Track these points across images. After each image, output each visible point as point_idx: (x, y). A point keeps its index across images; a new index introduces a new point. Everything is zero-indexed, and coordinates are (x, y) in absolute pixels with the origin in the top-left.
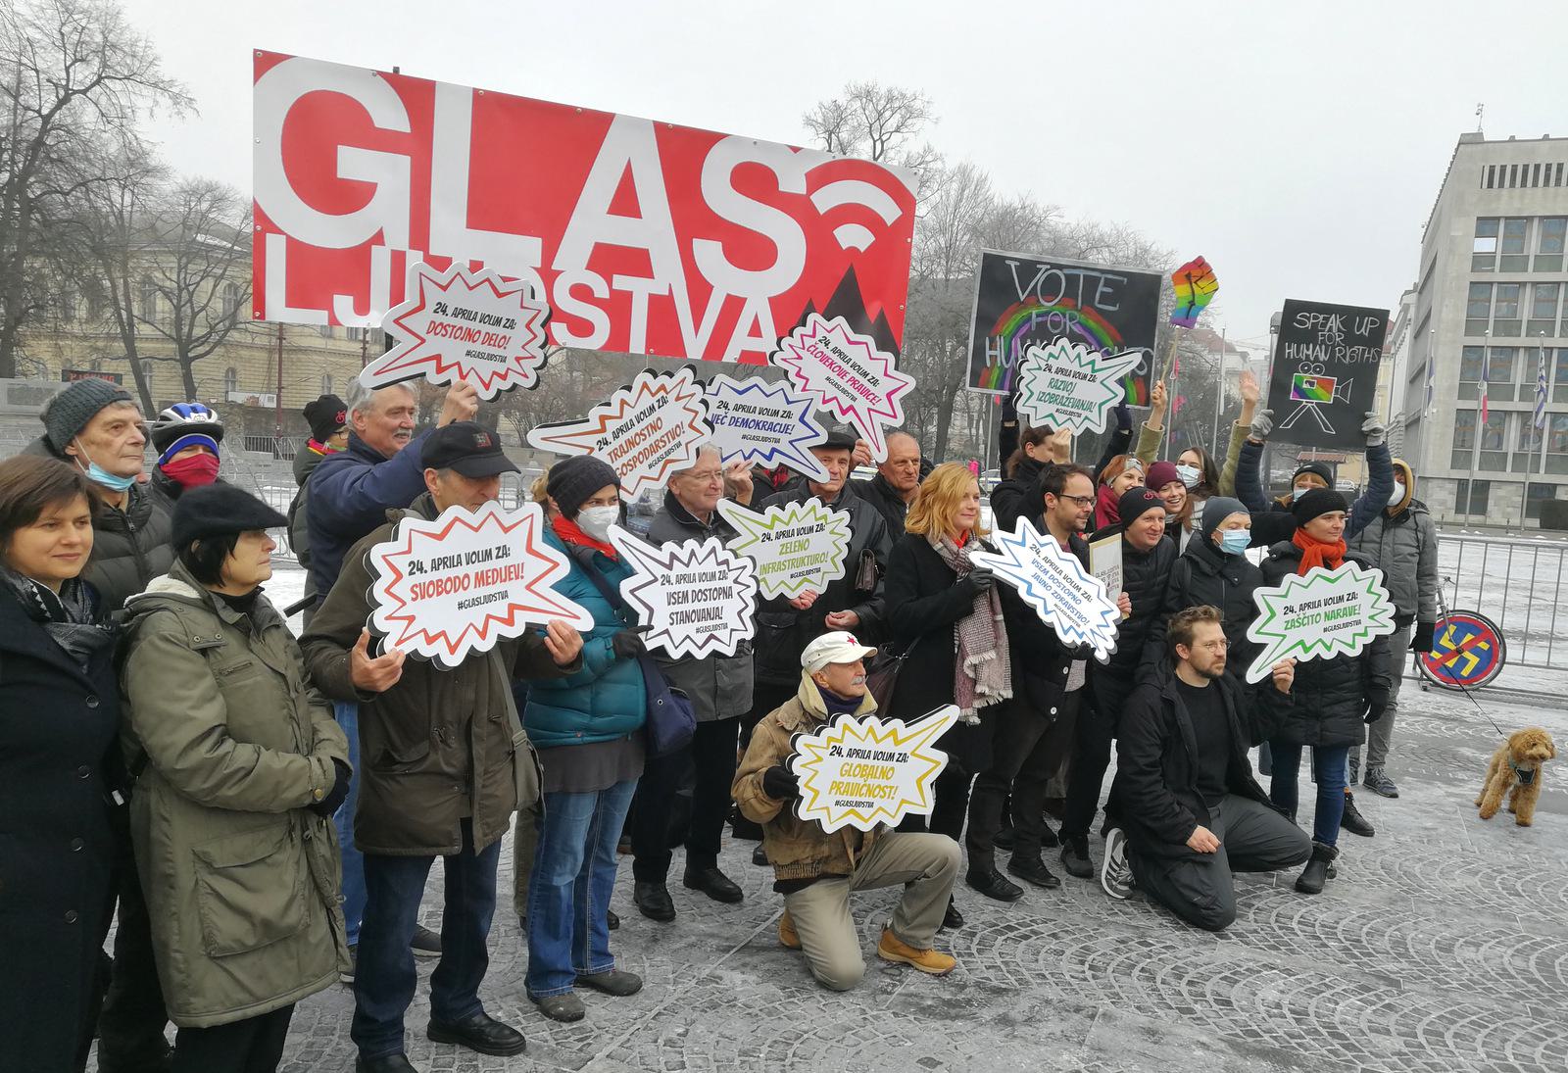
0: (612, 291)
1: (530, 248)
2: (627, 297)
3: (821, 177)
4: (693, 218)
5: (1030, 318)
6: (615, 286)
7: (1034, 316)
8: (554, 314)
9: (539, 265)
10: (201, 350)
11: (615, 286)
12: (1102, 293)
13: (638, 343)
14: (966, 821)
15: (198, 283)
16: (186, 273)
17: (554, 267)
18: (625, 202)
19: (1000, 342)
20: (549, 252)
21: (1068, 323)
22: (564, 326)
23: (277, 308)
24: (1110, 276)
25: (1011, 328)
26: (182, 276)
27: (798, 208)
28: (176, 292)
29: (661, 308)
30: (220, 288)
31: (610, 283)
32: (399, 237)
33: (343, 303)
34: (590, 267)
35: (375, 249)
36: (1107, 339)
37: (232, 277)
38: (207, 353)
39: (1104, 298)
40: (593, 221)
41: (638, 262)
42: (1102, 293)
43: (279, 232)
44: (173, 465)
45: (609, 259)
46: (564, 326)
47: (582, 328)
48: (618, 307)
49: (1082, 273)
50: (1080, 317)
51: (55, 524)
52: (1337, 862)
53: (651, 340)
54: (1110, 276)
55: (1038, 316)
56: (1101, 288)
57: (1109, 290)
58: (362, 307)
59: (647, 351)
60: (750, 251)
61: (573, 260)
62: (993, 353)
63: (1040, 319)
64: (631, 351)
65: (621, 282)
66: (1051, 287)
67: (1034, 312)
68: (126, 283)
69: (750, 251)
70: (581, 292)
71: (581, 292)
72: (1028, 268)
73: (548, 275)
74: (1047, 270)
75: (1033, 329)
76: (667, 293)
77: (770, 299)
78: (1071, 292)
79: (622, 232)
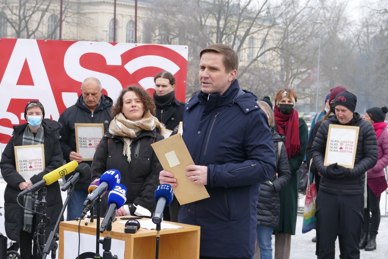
14: (32, 252)
15: (30, 16)
16: (25, 9)
18: (25, 78)
26: (22, 12)
28: (18, 22)
30: (45, 19)
34: (9, 110)
37: (53, 10)
52: (329, 93)
79: (25, 93)
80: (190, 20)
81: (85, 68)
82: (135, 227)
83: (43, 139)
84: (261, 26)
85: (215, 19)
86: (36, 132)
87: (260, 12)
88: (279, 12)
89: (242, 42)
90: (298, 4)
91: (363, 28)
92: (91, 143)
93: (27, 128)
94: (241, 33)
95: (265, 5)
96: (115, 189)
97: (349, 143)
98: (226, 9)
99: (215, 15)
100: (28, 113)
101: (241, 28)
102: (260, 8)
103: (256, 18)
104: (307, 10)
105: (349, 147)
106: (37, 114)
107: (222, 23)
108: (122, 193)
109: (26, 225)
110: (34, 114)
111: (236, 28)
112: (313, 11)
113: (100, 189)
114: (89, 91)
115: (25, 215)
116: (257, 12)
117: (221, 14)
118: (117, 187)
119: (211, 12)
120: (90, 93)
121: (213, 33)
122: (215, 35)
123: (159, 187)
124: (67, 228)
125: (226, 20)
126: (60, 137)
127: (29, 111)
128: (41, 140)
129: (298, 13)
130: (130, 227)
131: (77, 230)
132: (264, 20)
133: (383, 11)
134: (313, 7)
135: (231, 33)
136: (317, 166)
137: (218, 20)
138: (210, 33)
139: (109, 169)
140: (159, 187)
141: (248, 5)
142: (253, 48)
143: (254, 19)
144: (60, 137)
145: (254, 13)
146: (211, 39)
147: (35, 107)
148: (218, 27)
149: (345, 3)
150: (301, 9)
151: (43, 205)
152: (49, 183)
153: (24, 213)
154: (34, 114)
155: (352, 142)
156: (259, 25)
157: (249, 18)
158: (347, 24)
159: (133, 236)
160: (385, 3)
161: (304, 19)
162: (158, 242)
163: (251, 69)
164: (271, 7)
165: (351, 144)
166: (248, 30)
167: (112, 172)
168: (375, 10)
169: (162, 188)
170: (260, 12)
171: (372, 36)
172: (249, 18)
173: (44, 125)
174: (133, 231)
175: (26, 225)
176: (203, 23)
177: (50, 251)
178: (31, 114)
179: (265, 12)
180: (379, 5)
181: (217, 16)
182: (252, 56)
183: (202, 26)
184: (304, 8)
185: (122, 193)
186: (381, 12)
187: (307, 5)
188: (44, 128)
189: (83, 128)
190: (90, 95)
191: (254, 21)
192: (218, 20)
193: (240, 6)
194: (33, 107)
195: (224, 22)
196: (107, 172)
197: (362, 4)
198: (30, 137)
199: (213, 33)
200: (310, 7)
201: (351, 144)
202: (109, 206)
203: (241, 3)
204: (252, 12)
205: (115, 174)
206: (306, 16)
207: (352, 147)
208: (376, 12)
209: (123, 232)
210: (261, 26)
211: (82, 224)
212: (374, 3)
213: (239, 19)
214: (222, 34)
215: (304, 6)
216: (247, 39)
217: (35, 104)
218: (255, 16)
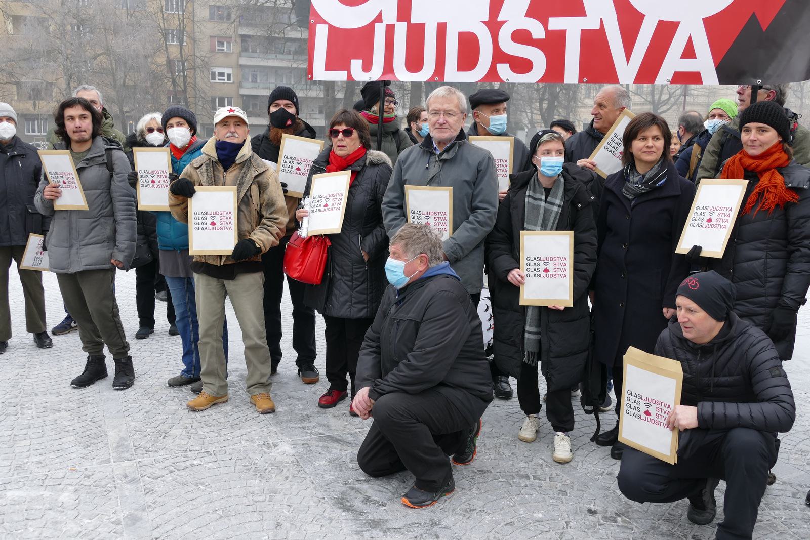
0: (547, 32)
6: (550, 28)
8: (499, 56)
9: (487, 19)
10: (665, 108)
11: (550, 28)
13: (572, 73)
17: (499, 19)
22: (507, 66)
23: (320, 73)
29: (594, 42)
31: (545, 24)
32: (390, 16)
33: (356, 65)
35: (377, 25)
38: (668, 110)
43: (325, 22)
44: (394, 166)
46: (507, 66)
47: (522, 65)
48: (554, 45)
51: (645, 139)
58: (367, 67)
59: (581, 81)
64: (566, 81)
65: (556, 23)
70: (521, 37)
71: (521, 37)
73: (494, 25)
81: (364, 3)
83: (561, 200)
86: (550, 187)
93: (532, 180)
97: (502, 163)
105: (225, 220)
109: (528, 352)
110: (554, 153)
115: (526, 335)
126: (593, 198)
128: (558, 202)
136: (755, 376)
144: (593, 198)
147: (556, 140)
153: (524, 331)
154: (554, 153)
155: (506, 161)
165: (505, 164)
173: (566, 174)
175: (528, 352)
188: (565, 180)
194: (553, 140)
198: (538, 196)
201: (505, 164)
207: (565, 273)
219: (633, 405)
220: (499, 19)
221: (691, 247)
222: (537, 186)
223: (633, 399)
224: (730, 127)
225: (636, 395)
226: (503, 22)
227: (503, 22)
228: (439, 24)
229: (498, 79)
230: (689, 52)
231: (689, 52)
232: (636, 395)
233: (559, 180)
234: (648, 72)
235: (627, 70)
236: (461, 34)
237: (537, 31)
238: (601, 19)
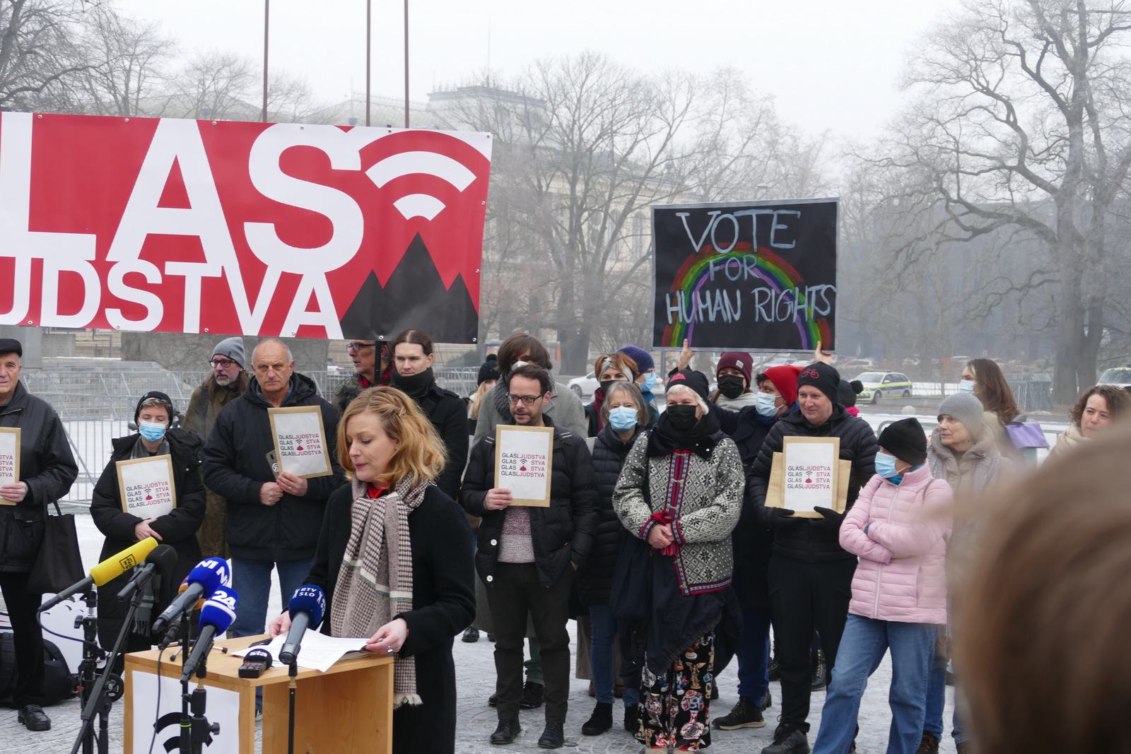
0: (164, 277)
1: (85, 244)
2: (181, 281)
3: (373, 154)
4: (242, 205)
5: (707, 269)
6: (167, 272)
7: (711, 266)
8: (108, 300)
11: (167, 272)
12: (777, 231)
17: (109, 259)
19: (681, 297)
20: (103, 247)
21: (746, 268)
24: (783, 212)
25: (690, 281)
27: (352, 183)
29: (215, 290)
31: (162, 269)
36: (787, 281)
39: (780, 236)
40: (143, 215)
41: (190, 248)
42: (777, 231)
45: (159, 248)
47: (135, 311)
48: (172, 291)
49: (754, 213)
50: (757, 260)
53: (204, 320)
54: (783, 212)
55: (715, 265)
56: (775, 226)
57: (783, 227)
60: (306, 229)
61: (126, 250)
62: (674, 309)
63: (718, 268)
65: (173, 268)
66: (724, 231)
67: (711, 261)
68: (696, 585)
69: (306, 229)
70: (134, 280)
71: (134, 280)
72: (699, 216)
73: (102, 266)
74: (718, 216)
75: (712, 279)
76: (219, 275)
77: (30, 230)
78: (745, 237)
79: (173, 223)
80: (517, 184)
82: (263, 665)
84: (657, 191)
85: (566, 180)
87: (652, 166)
88: (690, 166)
89: (620, 223)
90: (725, 150)
91: (852, 193)
92: (302, 445)
93: (136, 445)
94: (617, 207)
95: (663, 153)
96: (214, 598)
98: (586, 161)
99: (566, 174)
100: (141, 415)
101: (616, 198)
102: (653, 158)
103: (646, 177)
104: (742, 160)
106: (159, 419)
107: (580, 187)
108: (226, 605)
110: (153, 419)
111: (607, 198)
112: (754, 163)
113: (185, 597)
114: (267, 360)
116: (647, 167)
117: (578, 171)
118: (217, 592)
119: (558, 169)
120: (270, 363)
121: (563, 208)
122: (567, 213)
123: (297, 591)
124: (137, 665)
125: (587, 185)
127: (143, 412)
129: (726, 168)
130: (252, 666)
131: (156, 670)
132: (661, 182)
133: (885, 161)
134: (755, 154)
135: (597, 207)
137: (573, 183)
138: (556, 209)
139: (206, 558)
140: (297, 591)
141: (628, 153)
142: (641, 235)
143: (642, 180)
145: (641, 168)
146: (560, 218)
148: (573, 197)
149: (818, 145)
150: (732, 159)
151: (90, 624)
152: (299, 487)
154: (153, 419)
156: (652, 190)
157: (632, 178)
158: (820, 187)
159: (255, 682)
160: (889, 147)
161: (738, 178)
162: (292, 699)
163: (636, 277)
164: (675, 156)
166: (631, 202)
167: (212, 564)
168: (871, 160)
169: (301, 594)
170: (652, 166)
171: (869, 208)
172: (632, 178)
173: (171, 438)
174: (255, 674)
176: (544, 189)
177: (95, 715)
178: (148, 417)
179: (663, 165)
180: (877, 150)
181: (570, 175)
182: (640, 252)
183: (540, 194)
184: (737, 158)
185: (226, 605)
186: (881, 164)
187: (742, 151)
188: (171, 444)
189: (284, 417)
190: (270, 368)
191: (642, 183)
192: (573, 183)
193: (615, 156)
195: (583, 187)
196: (204, 564)
197: (845, 150)
199: (563, 208)
200: (748, 156)
202: (202, 629)
203: (615, 150)
204: (635, 166)
205: (217, 568)
206: (741, 173)
208: (870, 164)
209: (235, 674)
210: (657, 191)
211: (165, 659)
212: (867, 148)
213: (613, 181)
214: (581, 210)
215: (736, 154)
216: (629, 220)
217: (157, 401)
218: (643, 174)
219: (286, 446)
220: (109, 259)
221: (358, 155)
222: (141, 450)
223: (285, 441)
224: (349, 387)
225: (287, 437)
226: (113, 263)
227: (113, 263)
228: (33, 260)
229: (108, 326)
230: (313, 306)
231: (313, 306)
232: (287, 437)
233: (165, 445)
234: (273, 323)
235: (251, 323)
236: (62, 274)
237: (153, 275)
238: (223, 267)
